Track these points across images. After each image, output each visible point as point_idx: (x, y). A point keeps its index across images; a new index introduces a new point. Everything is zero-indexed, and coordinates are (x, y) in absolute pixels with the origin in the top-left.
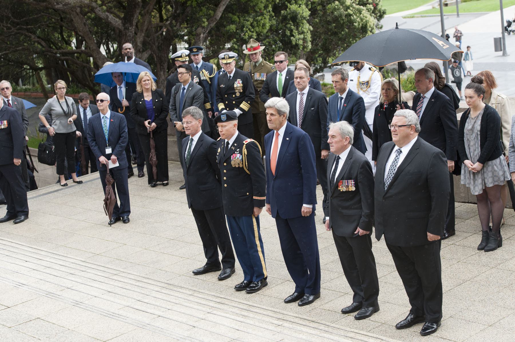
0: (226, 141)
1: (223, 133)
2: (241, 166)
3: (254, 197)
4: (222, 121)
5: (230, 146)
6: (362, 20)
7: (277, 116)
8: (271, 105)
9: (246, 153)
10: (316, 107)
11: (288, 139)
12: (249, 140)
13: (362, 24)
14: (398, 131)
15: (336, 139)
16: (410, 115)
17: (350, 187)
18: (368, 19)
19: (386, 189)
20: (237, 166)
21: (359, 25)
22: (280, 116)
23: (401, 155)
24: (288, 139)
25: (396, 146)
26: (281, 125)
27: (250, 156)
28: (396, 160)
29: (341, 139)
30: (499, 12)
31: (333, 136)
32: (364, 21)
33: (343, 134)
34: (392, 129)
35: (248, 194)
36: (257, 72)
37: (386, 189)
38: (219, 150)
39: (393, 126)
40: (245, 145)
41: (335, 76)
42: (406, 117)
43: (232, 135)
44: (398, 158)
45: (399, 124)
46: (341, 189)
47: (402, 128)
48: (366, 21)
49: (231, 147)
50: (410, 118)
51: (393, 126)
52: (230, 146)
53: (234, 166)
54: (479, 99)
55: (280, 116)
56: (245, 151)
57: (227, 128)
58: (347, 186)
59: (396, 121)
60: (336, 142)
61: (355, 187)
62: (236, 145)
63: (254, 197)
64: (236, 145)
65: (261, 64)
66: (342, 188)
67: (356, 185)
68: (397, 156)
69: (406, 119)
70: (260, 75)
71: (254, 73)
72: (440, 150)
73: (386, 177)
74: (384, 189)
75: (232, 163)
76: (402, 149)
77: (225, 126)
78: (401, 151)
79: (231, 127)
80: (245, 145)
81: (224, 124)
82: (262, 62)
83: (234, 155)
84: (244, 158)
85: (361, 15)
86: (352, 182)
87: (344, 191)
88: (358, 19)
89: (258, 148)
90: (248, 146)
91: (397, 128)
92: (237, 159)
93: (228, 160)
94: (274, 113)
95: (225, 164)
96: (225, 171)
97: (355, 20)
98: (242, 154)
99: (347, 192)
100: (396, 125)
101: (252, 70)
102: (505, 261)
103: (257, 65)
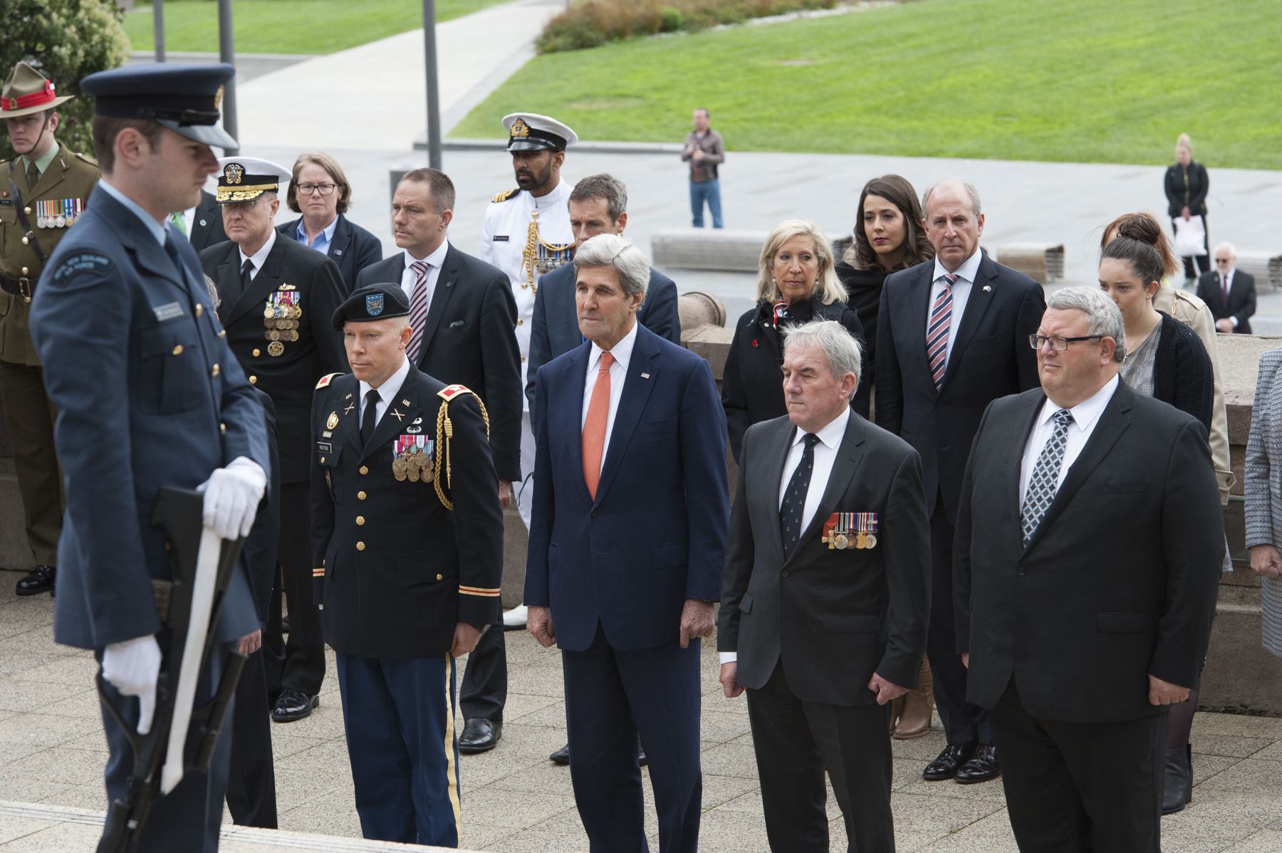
0: (365, 388)
1: (365, 358)
2: (427, 477)
3: (464, 590)
4: (366, 317)
5: (381, 409)
6: (84, 33)
7: (617, 298)
8: (603, 255)
9: (449, 433)
10: (470, 317)
11: (646, 376)
12: (458, 389)
13: (87, 54)
14: (1062, 356)
15: (806, 385)
16: (1099, 304)
17: (860, 536)
18: (108, 31)
19: (1028, 536)
20: (414, 478)
21: (74, 54)
22: (627, 297)
23: (1072, 430)
24: (646, 376)
25: (1049, 401)
26: (623, 332)
27: (463, 444)
28: (1057, 444)
29: (831, 380)
30: (418, 35)
31: (805, 373)
32: (96, 38)
33: (835, 364)
34: (1043, 348)
35: (439, 577)
36: (44, 196)
37: (1028, 536)
38: (333, 420)
39: (1045, 338)
40: (445, 405)
41: (587, 204)
42: (1087, 311)
43: (394, 369)
44: (1063, 441)
45: (1068, 332)
46: (831, 540)
47: (1077, 347)
48: (103, 40)
49: (390, 409)
50: (1101, 313)
51: (1045, 338)
52: (381, 409)
53: (402, 479)
54: (1145, 295)
55: (627, 297)
56: (446, 425)
57: (382, 341)
58: (853, 534)
59: (1056, 324)
60: (816, 391)
61: (876, 535)
62: (407, 403)
63: (464, 590)
64: (407, 403)
65: (55, 162)
66: (836, 540)
67: (880, 532)
68: (1059, 434)
69: (1087, 318)
70: (59, 209)
71: (32, 204)
72: (1196, 420)
73: (1023, 498)
74: (1023, 535)
75: (398, 466)
76: (1074, 412)
77: (379, 334)
78: (1071, 419)
79: (394, 341)
80: (445, 405)
81: (376, 326)
82: (58, 156)
83: (405, 439)
84: (439, 449)
85: (81, 14)
86: (868, 520)
87: (841, 547)
88: (71, 31)
89: (480, 413)
90: (456, 407)
91: (1059, 348)
92: (416, 452)
93: (382, 459)
94: (610, 284)
95: (364, 470)
96: (362, 495)
97: (54, 29)
98: (432, 436)
99: (851, 553)
100: (1056, 337)
101: (24, 190)
102: (1228, 843)
103: (42, 167)
